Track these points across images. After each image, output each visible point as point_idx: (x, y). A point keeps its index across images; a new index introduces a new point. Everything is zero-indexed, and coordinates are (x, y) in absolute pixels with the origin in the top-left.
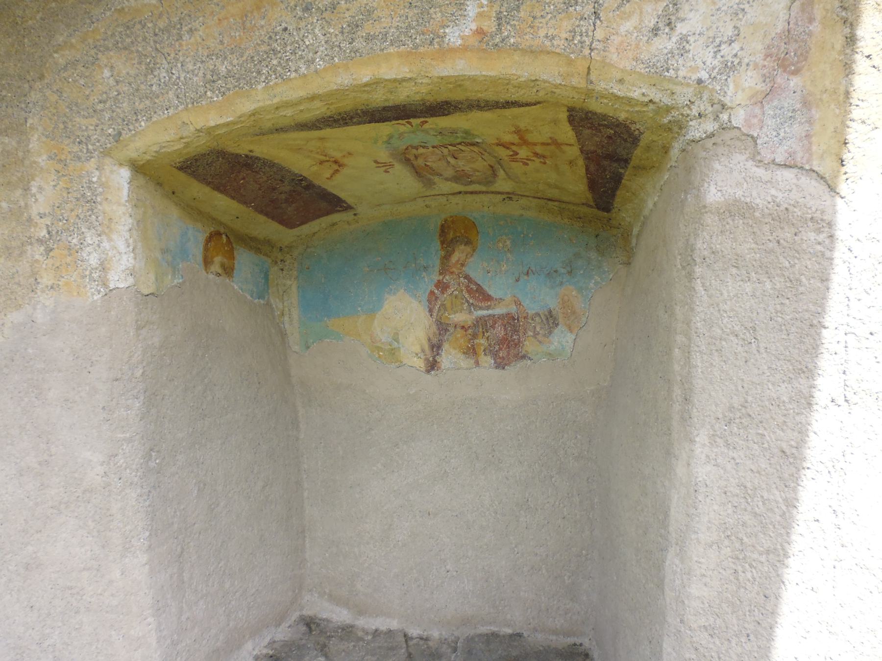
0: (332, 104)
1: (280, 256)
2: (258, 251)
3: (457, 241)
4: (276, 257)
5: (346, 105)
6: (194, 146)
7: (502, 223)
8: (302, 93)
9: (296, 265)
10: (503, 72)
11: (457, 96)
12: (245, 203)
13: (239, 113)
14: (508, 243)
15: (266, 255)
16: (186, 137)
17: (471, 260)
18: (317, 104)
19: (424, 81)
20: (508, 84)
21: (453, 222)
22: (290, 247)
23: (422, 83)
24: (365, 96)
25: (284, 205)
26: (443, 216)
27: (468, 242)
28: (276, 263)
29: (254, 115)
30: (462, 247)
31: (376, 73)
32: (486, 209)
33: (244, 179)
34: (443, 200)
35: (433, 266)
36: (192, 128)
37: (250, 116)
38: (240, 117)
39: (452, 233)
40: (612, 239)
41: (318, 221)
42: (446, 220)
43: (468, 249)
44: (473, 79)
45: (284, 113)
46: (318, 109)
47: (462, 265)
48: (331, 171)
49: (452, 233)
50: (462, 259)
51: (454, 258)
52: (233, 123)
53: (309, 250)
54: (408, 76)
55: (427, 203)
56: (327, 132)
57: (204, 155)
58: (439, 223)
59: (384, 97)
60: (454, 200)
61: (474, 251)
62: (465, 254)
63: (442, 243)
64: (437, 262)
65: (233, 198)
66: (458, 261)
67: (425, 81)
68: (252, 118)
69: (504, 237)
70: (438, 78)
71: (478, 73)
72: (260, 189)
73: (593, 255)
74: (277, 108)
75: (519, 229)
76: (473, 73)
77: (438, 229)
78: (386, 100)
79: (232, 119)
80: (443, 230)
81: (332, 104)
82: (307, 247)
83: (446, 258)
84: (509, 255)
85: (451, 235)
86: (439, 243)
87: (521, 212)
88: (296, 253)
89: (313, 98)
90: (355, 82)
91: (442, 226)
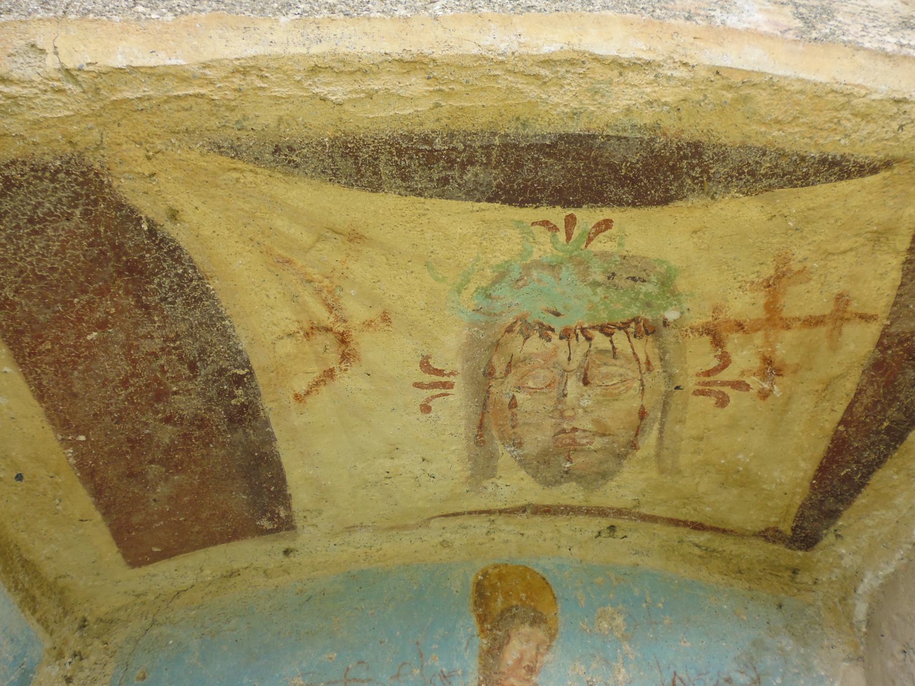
0: (450, 94)
1: (75, 643)
2: (30, 603)
3: (514, 616)
4: (66, 642)
5: (482, 110)
6: (30, 116)
7: (599, 579)
8: (394, 48)
9: (109, 669)
10: (841, 79)
11: (728, 131)
12: (63, 423)
13: (206, 57)
14: (619, 620)
15: (43, 622)
16: (19, 82)
17: (548, 657)
18: (417, 85)
19: (676, 74)
20: (843, 106)
21: (501, 577)
22: (108, 622)
23: (669, 78)
24: (533, 91)
25: (154, 470)
26: (480, 565)
27: (537, 620)
28: (61, 655)
29: (244, 71)
30: (526, 629)
31: (575, 41)
32: (565, 551)
33: (102, 325)
34: (480, 525)
35: (465, 673)
36: (51, 62)
37: (235, 71)
38: (206, 66)
39: (500, 599)
40: (810, 611)
41: (200, 556)
42: (485, 574)
43: (540, 633)
44: (774, 85)
45: (322, 90)
46: (411, 106)
47: (531, 670)
48: (316, 371)
49: (500, 599)
50: (527, 656)
51: (513, 651)
52: (182, 76)
53: (155, 631)
54: (646, 57)
55: (448, 536)
56: (382, 210)
57: (39, 171)
58: (472, 579)
59: (575, 104)
60: (507, 529)
61: (552, 637)
62: (532, 645)
63: (482, 619)
64: (474, 665)
65: (41, 394)
66: (520, 660)
67: (682, 73)
68: (237, 81)
69: (609, 609)
70: (709, 69)
71: (789, 73)
72: (125, 383)
73: (788, 643)
74: (315, 70)
75: (636, 592)
76: (781, 72)
77: (471, 588)
78: (575, 114)
79: (183, 63)
80: (482, 593)
81: (450, 94)
82: (154, 623)
83: (492, 653)
84: (626, 647)
85: (499, 604)
86: (474, 620)
87: (635, 559)
88: (119, 637)
89: (412, 64)
90: (523, 50)
91: (479, 585)
